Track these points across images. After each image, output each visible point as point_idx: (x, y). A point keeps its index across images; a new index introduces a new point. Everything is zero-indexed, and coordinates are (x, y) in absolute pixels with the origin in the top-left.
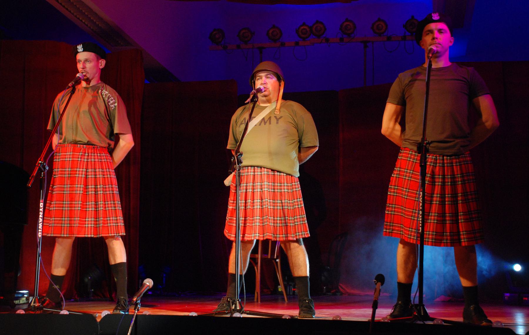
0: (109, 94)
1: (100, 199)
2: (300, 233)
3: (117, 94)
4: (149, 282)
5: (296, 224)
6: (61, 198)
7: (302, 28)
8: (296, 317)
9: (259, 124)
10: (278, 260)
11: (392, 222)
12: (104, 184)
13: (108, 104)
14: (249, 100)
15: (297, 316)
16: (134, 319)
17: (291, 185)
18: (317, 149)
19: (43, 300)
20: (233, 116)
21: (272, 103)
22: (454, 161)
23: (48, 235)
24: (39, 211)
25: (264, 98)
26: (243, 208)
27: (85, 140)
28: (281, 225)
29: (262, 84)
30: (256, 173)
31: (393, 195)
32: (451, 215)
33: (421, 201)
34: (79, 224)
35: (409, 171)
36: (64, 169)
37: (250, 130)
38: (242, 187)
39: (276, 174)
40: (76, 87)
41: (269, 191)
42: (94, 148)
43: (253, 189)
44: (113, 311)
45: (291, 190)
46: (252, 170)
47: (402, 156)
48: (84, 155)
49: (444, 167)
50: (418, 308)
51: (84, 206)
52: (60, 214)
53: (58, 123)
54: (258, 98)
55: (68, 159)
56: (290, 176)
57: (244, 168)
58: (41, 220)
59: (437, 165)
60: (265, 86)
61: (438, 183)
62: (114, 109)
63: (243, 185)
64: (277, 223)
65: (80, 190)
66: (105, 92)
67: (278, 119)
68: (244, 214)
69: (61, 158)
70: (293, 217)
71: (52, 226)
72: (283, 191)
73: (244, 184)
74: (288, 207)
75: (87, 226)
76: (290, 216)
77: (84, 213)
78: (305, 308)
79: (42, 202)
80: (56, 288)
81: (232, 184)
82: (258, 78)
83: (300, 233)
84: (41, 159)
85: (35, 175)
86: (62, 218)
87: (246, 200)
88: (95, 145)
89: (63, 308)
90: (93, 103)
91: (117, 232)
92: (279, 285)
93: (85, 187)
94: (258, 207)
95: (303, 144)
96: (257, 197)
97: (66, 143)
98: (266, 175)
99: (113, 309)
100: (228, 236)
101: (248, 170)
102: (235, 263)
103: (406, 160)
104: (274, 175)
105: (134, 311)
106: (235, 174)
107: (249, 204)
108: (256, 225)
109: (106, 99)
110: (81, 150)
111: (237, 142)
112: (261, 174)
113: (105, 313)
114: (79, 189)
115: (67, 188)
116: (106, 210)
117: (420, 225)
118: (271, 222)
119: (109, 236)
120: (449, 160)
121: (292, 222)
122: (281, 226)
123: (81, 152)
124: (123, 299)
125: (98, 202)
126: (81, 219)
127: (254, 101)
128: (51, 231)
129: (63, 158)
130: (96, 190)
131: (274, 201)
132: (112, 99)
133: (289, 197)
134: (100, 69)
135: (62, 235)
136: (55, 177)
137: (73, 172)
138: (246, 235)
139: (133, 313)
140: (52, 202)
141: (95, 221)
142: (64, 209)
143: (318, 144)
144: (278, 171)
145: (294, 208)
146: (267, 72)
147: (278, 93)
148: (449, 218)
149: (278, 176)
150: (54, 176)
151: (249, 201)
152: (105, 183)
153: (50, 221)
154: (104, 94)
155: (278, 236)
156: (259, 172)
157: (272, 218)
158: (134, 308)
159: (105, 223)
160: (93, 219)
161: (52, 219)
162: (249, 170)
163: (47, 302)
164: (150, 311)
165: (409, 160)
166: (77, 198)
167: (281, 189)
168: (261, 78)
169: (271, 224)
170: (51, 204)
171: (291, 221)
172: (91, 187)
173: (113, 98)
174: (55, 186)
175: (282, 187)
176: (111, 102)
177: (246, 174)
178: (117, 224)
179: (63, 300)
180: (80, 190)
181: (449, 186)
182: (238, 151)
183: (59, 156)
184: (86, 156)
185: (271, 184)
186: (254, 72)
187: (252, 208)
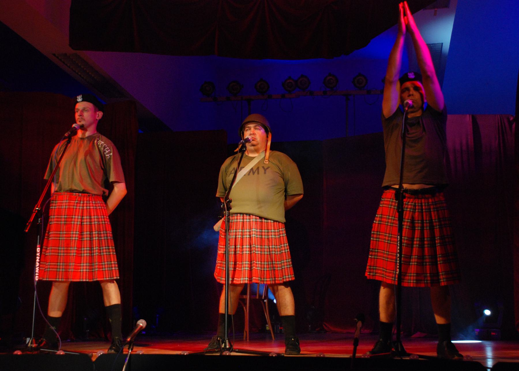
0: (105, 145)
1: (95, 244)
2: (287, 277)
3: (113, 144)
4: (142, 323)
5: (283, 267)
6: (57, 243)
7: (288, 81)
8: (283, 354)
9: (248, 174)
10: (265, 301)
11: (375, 266)
12: (99, 230)
13: (104, 154)
14: (237, 149)
15: (283, 353)
16: (128, 358)
17: (278, 231)
18: (301, 196)
19: (40, 341)
20: (222, 166)
21: (260, 153)
22: (431, 207)
23: (44, 279)
24: (36, 256)
25: (252, 148)
26: (233, 253)
27: (81, 188)
28: (268, 269)
29: (250, 135)
30: (245, 220)
31: (375, 240)
32: (430, 257)
33: (399, 245)
34: (74, 269)
35: (390, 217)
36: (60, 217)
37: (239, 180)
38: (232, 233)
39: (264, 221)
40: (72, 138)
41: (257, 237)
42: (89, 196)
43: (242, 235)
44: (108, 350)
45: (278, 236)
46: (241, 218)
47: (383, 204)
48: (80, 203)
49: (422, 212)
50: (396, 344)
51: (79, 252)
52: (55, 259)
53: (54, 171)
54: (246, 147)
55: (64, 207)
56: (278, 223)
57: (233, 215)
58: (38, 264)
59: (417, 211)
60: (253, 136)
61: (418, 228)
62: (109, 158)
63: (233, 231)
64: (264, 268)
65: (75, 237)
66: (101, 142)
67: (265, 170)
68: (234, 259)
69: (57, 206)
70: (280, 262)
71: (47, 271)
72: (270, 237)
73: (234, 230)
74: (276, 252)
75: (82, 270)
76: (278, 261)
77: (78, 259)
78: (290, 346)
79: (39, 247)
80: (53, 330)
81: (221, 229)
82: (247, 128)
83: (287, 277)
84: (38, 205)
85: (32, 221)
86: (58, 263)
87: (235, 246)
88: (89, 193)
89: (60, 348)
90: (89, 153)
91: (112, 276)
92: (267, 324)
93: (80, 234)
94: (246, 252)
95: (288, 192)
96: (246, 243)
97: (62, 191)
98: (254, 222)
99: (108, 348)
100: (218, 279)
101: (237, 216)
102: (225, 303)
103: (387, 207)
104: (262, 222)
105: (128, 350)
106: (224, 221)
107: (238, 249)
108: (245, 270)
109: (102, 149)
110: (76, 198)
111: (226, 190)
112: (249, 221)
113: (100, 353)
114: (75, 235)
115: (63, 234)
116: (101, 255)
117: (398, 267)
118: (259, 266)
119: (104, 280)
120: (428, 206)
121: (279, 266)
122: (268, 270)
123: (77, 200)
124: (118, 339)
125: (93, 248)
126: (76, 264)
127: (242, 151)
128: (47, 276)
129: (59, 206)
130: (92, 236)
131: (262, 247)
132: (107, 149)
133: (276, 242)
134: (97, 120)
135: (57, 280)
136: (51, 224)
137: (69, 220)
138: (235, 279)
139: (127, 353)
140: (49, 247)
141: (90, 266)
142: (60, 254)
143: (301, 191)
144: (265, 219)
145: (281, 253)
146: (255, 124)
147: (266, 143)
148: (429, 260)
149: (266, 223)
150: (50, 222)
151: (239, 246)
152: (100, 229)
153: (46, 266)
154: (99, 144)
155: (265, 279)
156: (248, 219)
157: (260, 262)
158: (128, 348)
159: (100, 268)
160: (88, 264)
161: (47, 264)
162: (239, 218)
163: (44, 342)
164: (143, 350)
165: (390, 207)
166: (72, 244)
167: (268, 235)
168: (250, 129)
169: (258, 268)
170: (46, 249)
171: (278, 266)
172: (86, 233)
173: (108, 148)
174: (51, 232)
175: (269, 233)
176: (107, 152)
177: (235, 221)
178: (111, 268)
179: (59, 341)
180: (75, 237)
181: (428, 230)
182: (227, 198)
183: (55, 203)
184: (81, 204)
185: (258, 230)
186: (243, 123)
187: (241, 253)
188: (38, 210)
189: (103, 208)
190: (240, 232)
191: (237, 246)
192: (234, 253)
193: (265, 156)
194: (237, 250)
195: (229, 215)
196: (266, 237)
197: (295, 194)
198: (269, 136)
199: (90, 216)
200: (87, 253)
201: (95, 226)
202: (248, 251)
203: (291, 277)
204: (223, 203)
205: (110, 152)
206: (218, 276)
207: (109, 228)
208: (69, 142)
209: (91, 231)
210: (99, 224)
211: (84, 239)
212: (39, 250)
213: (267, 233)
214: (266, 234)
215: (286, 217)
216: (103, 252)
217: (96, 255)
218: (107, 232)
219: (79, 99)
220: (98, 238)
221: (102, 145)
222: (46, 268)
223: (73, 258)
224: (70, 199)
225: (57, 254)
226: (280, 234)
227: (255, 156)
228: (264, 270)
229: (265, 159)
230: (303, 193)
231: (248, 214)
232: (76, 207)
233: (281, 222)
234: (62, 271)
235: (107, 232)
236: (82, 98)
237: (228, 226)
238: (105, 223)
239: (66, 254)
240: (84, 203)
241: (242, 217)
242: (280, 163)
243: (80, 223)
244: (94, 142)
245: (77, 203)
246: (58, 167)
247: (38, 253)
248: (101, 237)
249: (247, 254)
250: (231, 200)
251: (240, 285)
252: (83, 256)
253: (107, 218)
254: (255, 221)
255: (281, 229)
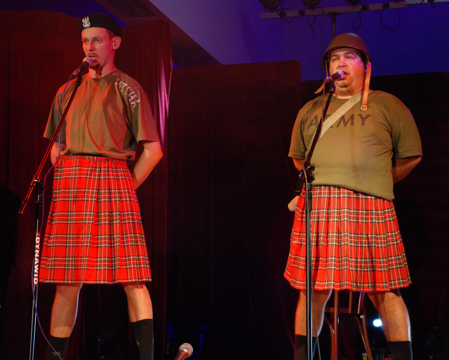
2: (397, 282)
6: (63, 230)
10: (362, 317)
17: (383, 212)
18: (419, 160)
21: (354, 94)
23: (46, 281)
24: (34, 249)
34: (88, 265)
39: (360, 197)
40: (83, 77)
46: (327, 191)
51: (94, 240)
56: (382, 200)
58: (37, 261)
67: (363, 120)
70: (386, 258)
76: (381, 257)
79: (38, 237)
81: (298, 208)
82: (334, 57)
83: (397, 282)
86: (66, 257)
87: (318, 233)
94: (333, 243)
101: (320, 190)
104: (358, 198)
107: (322, 239)
112: (338, 196)
125: (113, 235)
126: (90, 259)
132: (133, 93)
135: (66, 282)
137: (80, 194)
138: (317, 282)
144: (363, 194)
146: (345, 51)
147: (363, 78)
150: (54, 199)
167: (367, 219)
168: (339, 59)
172: (104, 214)
174: (55, 213)
175: (369, 216)
176: (132, 98)
177: (318, 196)
178: (139, 265)
183: (61, 171)
186: (328, 49)
188: (37, 182)
189: (127, 178)
190: (325, 213)
191: (320, 234)
192: (315, 244)
193: (362, 100)
194: (320, 240)
195: (310, 190)
196: (364, 221)
197: (410, 156)
198: (367, 67)
199: (109, 189)
200: (104, 265)
201: (116, 204)
202: (335, 241)
203: (403, 282)
204: (302, 171)
205: (136, 99)
206: (291, 278)
207: (137, 207)
208: (79, 83)
209: (111, 211)
210: (121, 201)
211: (101, 223)
212: (38, 240)
213: (365, 215)
214: (364, 216)
215: (396, 191)
216: (127, 242)
217: (117, 246)
218: (133, 213)
219: (86, 22)
220: (120, 221)
221: (125, 89)
222: (48, 265)
223: (86, 250)
224: (81, 165)
225: (65, 245)
226: (385, 217)
227: (322, 89)
228: (361, 271)
229: (361, 104)
230: (422, 155)
231: (337, 187)
232: (90, 177)
233: (387, 200)
234: (72, 269)
235: (133, 213)
236: (89, 23)
237: (309, 204)
238: (131, 199)
239: (76, 245)
240: (100, 171)
241: (328, 190)
242: (386, 110)
243: (96, 199)
244: (113, 85)
245: (91, 171)
246: (63, 122)
247: (38, 244)
248: (125, 220)
249: (334, 247)
250: (314, 166)
251: (326, 292)
252: (100, 247)
253: (133, 194)
254: (347, 197)
255: (386, 210)
